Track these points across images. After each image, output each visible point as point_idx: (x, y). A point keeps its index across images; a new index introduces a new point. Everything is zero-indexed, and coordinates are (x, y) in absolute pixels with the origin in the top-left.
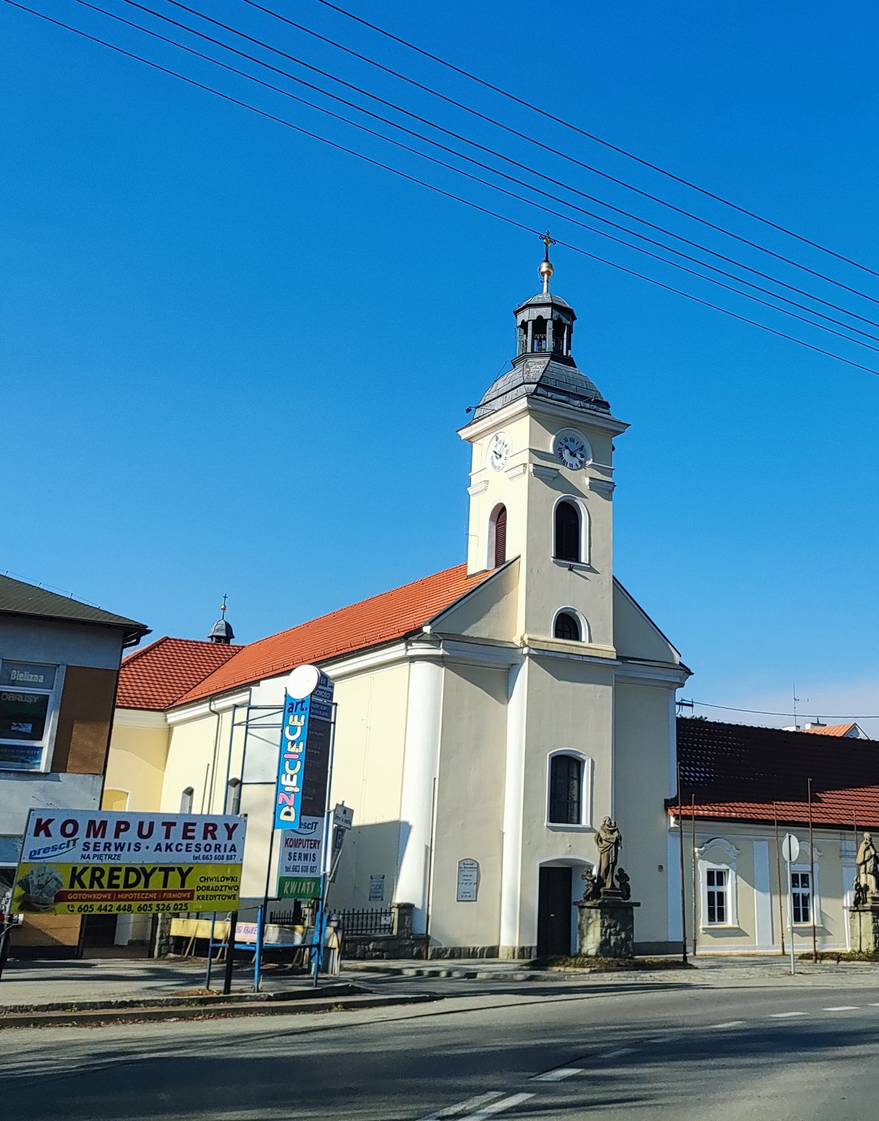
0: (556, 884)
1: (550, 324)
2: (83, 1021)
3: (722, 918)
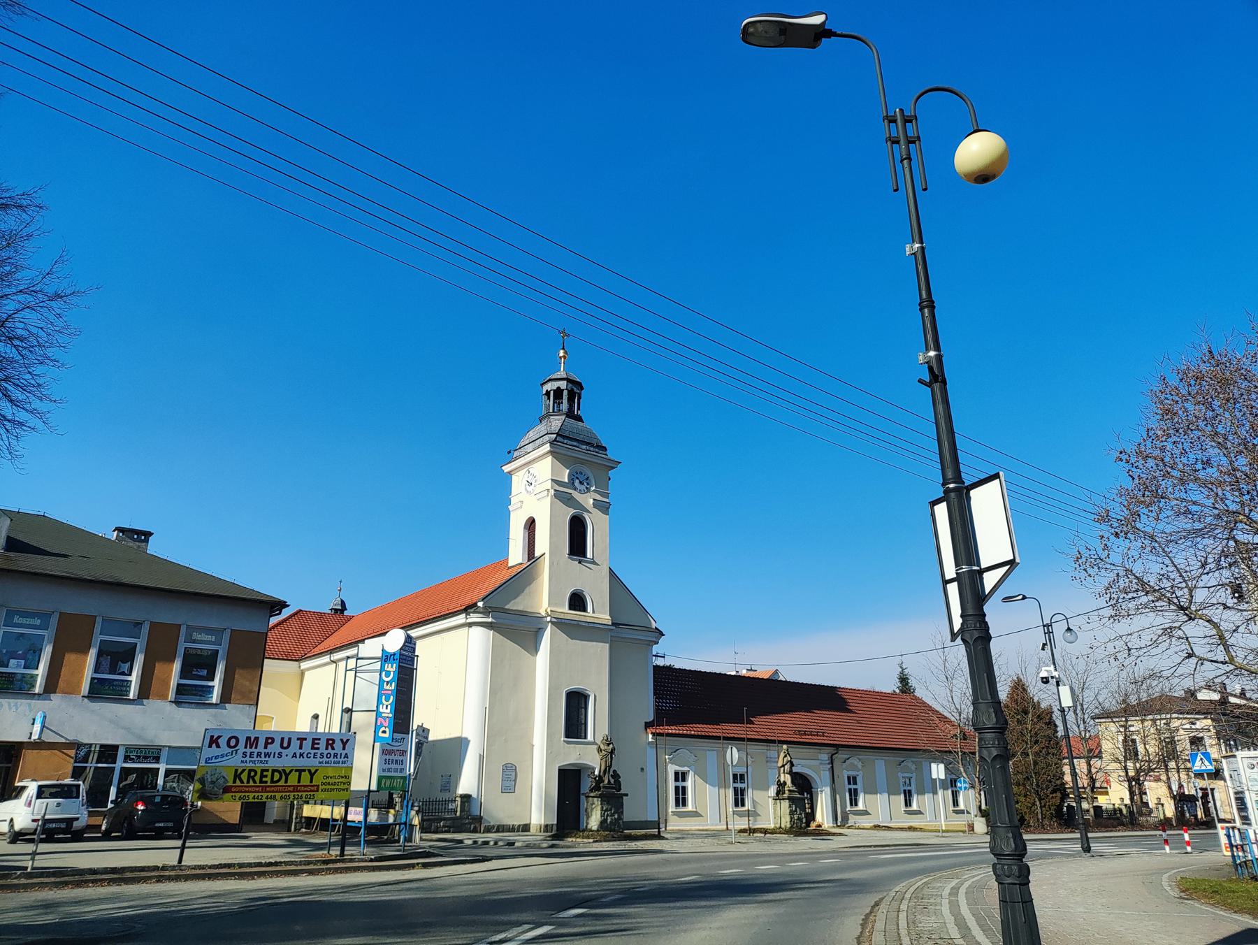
0: (569, 779)
1: (565, 393)
2: (242, 876)
3: (684, 804)
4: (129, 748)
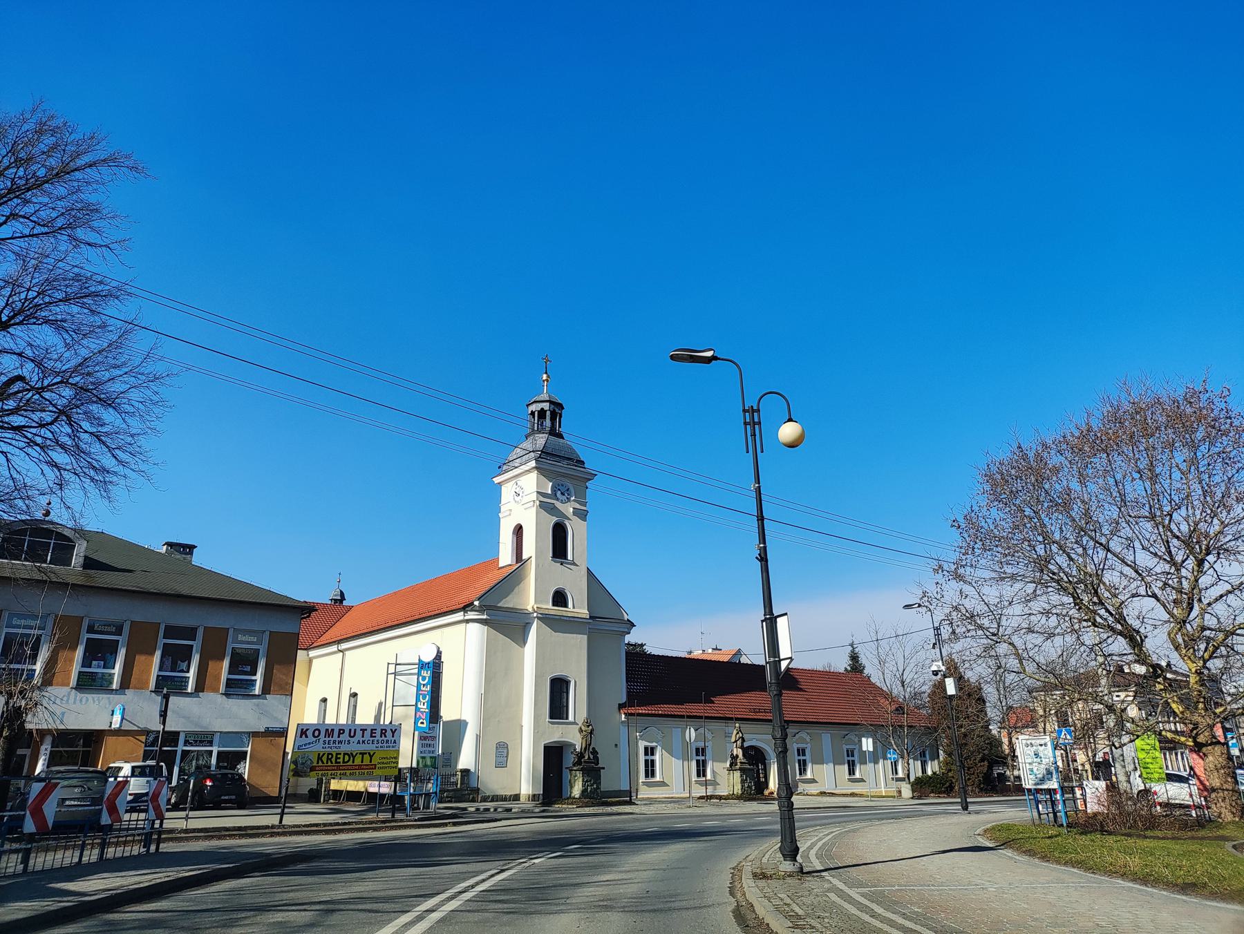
0: (553, 755)
1: (548, 413)
2: (327, 832)
3: (653, 775)
4: (187, 734)
